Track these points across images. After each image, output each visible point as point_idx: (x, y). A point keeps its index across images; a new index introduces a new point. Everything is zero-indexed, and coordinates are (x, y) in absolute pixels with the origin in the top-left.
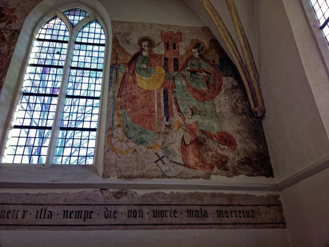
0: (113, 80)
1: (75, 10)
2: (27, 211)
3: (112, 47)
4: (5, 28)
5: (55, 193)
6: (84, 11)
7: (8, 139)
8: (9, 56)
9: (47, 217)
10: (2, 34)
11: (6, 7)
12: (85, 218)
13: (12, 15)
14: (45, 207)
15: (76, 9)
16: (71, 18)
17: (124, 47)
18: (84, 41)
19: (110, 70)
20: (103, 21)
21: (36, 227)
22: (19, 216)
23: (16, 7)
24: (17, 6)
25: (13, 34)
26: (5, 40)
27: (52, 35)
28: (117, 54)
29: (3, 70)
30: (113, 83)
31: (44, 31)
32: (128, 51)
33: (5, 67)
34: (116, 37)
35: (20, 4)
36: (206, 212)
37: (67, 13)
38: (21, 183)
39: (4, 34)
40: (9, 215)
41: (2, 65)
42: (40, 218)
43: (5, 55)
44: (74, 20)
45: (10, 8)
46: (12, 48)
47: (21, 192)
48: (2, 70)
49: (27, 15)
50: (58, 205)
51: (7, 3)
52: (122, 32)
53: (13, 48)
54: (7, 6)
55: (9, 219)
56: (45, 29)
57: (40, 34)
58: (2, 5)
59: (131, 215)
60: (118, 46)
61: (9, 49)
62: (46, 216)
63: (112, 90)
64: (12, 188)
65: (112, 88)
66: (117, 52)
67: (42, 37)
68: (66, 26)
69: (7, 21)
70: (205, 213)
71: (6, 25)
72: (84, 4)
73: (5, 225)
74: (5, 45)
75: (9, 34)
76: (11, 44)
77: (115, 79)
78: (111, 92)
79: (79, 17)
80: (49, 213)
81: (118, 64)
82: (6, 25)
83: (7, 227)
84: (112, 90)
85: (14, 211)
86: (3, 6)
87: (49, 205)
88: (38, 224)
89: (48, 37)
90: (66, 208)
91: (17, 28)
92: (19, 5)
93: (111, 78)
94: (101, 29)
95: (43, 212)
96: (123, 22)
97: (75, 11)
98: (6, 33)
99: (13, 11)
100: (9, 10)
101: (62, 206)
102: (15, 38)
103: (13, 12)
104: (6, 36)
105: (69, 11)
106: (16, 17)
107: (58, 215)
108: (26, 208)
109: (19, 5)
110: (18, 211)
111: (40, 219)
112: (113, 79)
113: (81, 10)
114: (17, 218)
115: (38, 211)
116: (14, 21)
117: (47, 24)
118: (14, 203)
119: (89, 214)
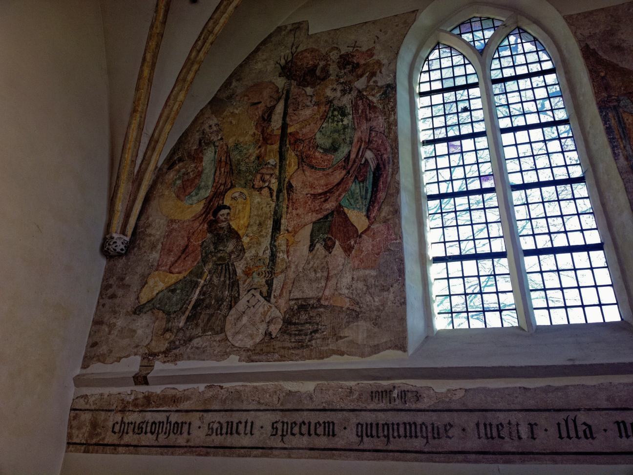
0: (616, 132)
1: (470, 21)
2: (536, 424)
3: (588, 66)
4: (367, 86)
5: (583, 385)
6: (489, 18)
7: (432, 284)
8: (393, 133)
9: (583, 436)
10: (367, 99)
11: (357, 50)
12: (283, 435)
13: (370, 61)
14: (572, 415)
15: (470, 19)
16: (467, 37)
17: (615, 61)
18: (508, 73)
19: (601, 115)
20: (538, 25)
21: (568, 456)
22: (523, 434)
23: (374, 45)
24: (375, 42)
25: (385, 93)
26: (375, 107)
27: (442, 79)
28: (603, 78)
29: (391, 160)
30: (620, 140)
31: (425, 77)
32: (626, 67)
33: (392, 154)
34: (587, 46)
35: (378, 38)
36: (589, 427)
37: (457, 31)
38: (507, 367)
39: (371, 98)
40: (501, 432)
41: (385, 152)
42: (569, 437)
43: (385, 134)
44: (474, 41)
45: (364, 49)
46: (392, 118)
47: (510, 385)
48: (389, 160)
49: (397, 54)
50: (598, 409)
51: (356, 42)
52: (598, 31)
53: (394, 119)
54: (358, 48)
55: (505, 440)
56: (425, 72)
57: (420, 83)
58: (349, 48)
59: (416, 432)
60: (599, 61)
61: (388, 122)
62: (581, 434)
63: (621, 154)
64: (489, 377)
65: (620, 151)
66: (602, 74)
67: (425, 88)
68: (499, 47)
69: (367, 74)
70: (219, 428)
71: (368, 81)
72: (487, 4)
73: (501, 453)
74: (378, 117)
75: (378, 95)
76: (387, 113)
77: (621, 130)
78: (622, 159)
79: (481, 32)
80: (584, 427)
81: (613, 97)
82: (368, 81)
83: (507, 457)
84: (623, 155)
85: (509, 423)
86: (351, 49)
87: (579, 410)
88: (568, 451)
89: (437, 86)
90: (619, 416)
91: (389, 80)
92: (376, 40)
93: (609, 130)
94: (535, 41)
95: (571, 425)
96: (591, 13)
97: (471, 22)
98: (373, 95)
99: (370, 53)
100: (363, 53)
101: (607, 412)
102: (392, 100)
103: (372, 55)
104: (375, 100)
105: (459, 26)
106: (379, 63)
107: (605, 430)
108: (533, 417)
109: (376, 40)
110: (518, 425)
111: (568, 440)
112: (616, 132)
113: (480, 18)
114: (520, 438)
115: (559, 424)
116: (378, 72)
117: (427, 62)
118: (504, 408)
119: (330, 429)
